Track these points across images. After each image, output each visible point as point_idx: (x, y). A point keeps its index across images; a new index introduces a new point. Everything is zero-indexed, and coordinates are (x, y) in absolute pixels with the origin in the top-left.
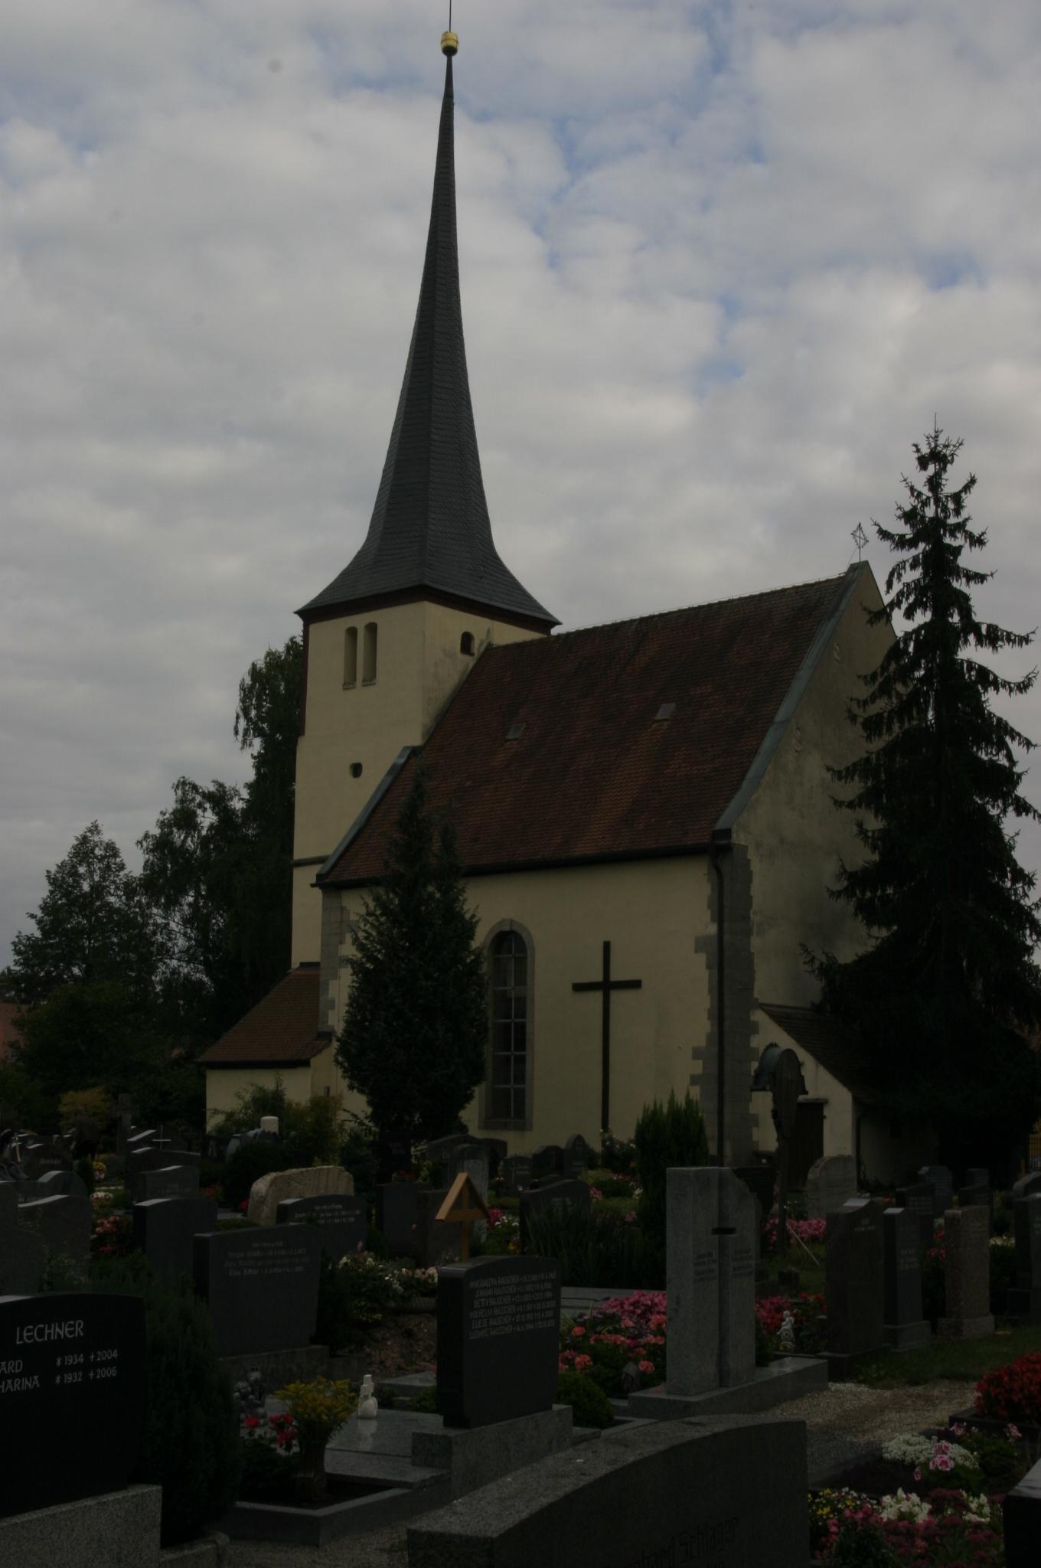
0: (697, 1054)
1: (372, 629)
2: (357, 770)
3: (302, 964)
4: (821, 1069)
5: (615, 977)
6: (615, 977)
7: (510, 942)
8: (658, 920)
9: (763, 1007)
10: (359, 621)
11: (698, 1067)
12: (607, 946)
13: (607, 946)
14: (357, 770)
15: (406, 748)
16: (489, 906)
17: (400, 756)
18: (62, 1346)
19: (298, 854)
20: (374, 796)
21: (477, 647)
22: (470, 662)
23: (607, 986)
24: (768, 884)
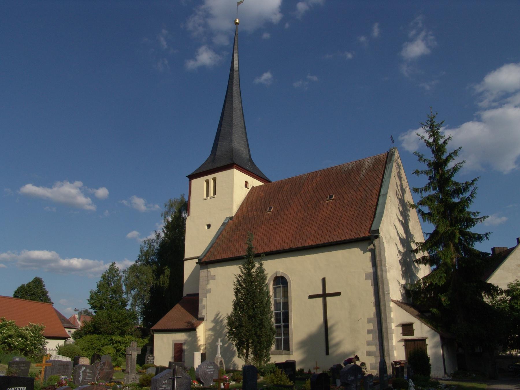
0: (370, 321)
1: (215, 180)
2: (209, 226)
3: (187, 295)
4: (423, 324)
5: (328, 291)
6: (328, 291)
7: (281, 281)
8: (346, 266)
9: (393, 301)
10: (210, 177)
11: (371, 326)
12: (324, 280)
13: (324, 280)
14: (209, 226)
15: (227, 218)
16: (272, 267)
17: (225, 220)
18: (46, 359)
19: (186, 256)
20: (216, 234)
21: (250, 186)
22: (248, 190)
23: (324, 295)
24: (391, 252)
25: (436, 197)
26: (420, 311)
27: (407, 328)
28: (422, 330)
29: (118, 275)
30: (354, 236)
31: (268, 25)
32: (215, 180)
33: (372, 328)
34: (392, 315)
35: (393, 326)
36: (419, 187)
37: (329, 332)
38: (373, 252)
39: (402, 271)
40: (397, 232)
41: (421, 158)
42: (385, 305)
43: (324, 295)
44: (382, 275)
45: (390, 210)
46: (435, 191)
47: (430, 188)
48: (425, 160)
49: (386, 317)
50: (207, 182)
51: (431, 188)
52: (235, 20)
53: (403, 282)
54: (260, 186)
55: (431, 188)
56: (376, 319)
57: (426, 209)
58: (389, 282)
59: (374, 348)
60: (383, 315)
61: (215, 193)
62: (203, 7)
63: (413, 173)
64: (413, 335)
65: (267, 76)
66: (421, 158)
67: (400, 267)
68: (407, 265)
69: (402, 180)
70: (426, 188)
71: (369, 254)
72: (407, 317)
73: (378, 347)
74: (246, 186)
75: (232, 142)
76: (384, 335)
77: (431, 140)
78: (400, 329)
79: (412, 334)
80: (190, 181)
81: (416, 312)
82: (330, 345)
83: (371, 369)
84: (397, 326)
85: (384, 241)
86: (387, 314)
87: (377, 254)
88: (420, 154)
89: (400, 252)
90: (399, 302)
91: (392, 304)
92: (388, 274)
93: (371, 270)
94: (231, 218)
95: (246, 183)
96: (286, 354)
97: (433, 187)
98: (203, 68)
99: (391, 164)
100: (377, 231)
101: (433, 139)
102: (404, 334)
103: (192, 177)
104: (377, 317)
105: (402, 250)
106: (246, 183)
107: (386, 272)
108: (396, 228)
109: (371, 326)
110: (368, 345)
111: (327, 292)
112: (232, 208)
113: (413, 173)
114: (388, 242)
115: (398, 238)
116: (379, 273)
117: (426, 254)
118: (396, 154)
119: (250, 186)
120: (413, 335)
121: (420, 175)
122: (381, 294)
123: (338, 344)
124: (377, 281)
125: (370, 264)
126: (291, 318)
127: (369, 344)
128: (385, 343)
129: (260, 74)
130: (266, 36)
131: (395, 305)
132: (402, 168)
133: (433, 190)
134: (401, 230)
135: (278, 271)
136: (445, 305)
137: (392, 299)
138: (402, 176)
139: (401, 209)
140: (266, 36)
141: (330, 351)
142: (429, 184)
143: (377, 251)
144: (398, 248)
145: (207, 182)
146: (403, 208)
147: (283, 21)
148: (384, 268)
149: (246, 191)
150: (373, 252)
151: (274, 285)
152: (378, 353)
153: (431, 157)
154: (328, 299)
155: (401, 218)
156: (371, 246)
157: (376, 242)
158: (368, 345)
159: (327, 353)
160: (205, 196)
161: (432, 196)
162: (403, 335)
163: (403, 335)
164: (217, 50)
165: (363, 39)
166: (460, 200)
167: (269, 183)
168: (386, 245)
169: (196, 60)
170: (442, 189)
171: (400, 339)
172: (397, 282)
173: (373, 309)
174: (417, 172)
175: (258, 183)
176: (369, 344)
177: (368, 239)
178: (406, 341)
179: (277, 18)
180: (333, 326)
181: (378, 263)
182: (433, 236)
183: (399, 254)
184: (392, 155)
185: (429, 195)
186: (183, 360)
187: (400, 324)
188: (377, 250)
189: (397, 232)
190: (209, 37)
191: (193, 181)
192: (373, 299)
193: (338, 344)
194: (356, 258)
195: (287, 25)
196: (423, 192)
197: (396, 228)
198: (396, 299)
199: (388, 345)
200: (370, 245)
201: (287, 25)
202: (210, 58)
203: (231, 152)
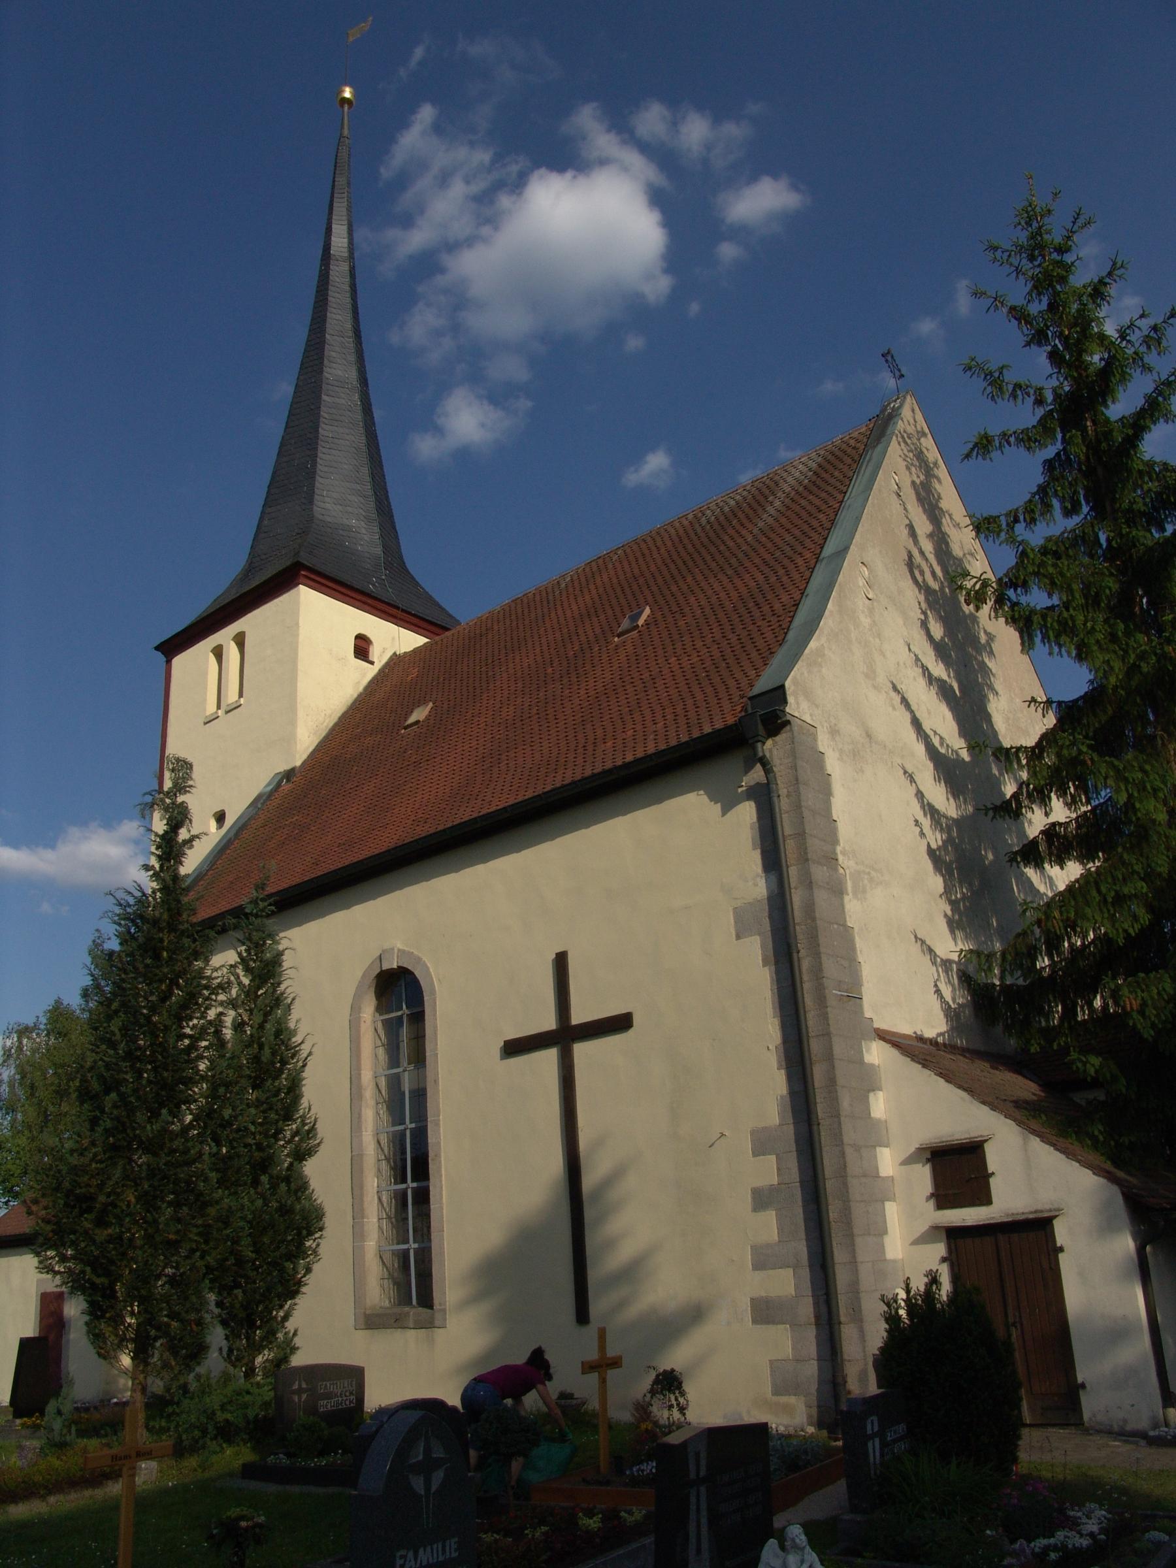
1: (240, 640)
4: (1035, 1143)
8: (652, 883)
9: (883, 1036)
10: (224, 636)
12: (561, 962)
13: (561, 962)
22: (370, 671)
23: (565, 1036)
25: (1081, 540)
26: (1046, 1085)
27: (957, 1169)
28: (1031, 1174)
31: (635, 312)
32: (240, 640)
33: (775, 1181)
34: (879, 1106)
35: (887, 1162)
36: (999, 507)
37: (589, 1214)
38: (764, 797)
39: (953, 903)
40: (916, 723)
41: (995, 382)
42: (829, 1057)
43: (565, 1036)
44: (810, 908)
45: (865, 621)
46: (1076, 520)
47: (1048, 507)
48: (1018, 386)
49: (836, 1115)
50: (218, 652)
51: (1056, 503)
53: (950, 947)
54: (416, 651)
55: (1056, 503)
56: (790, 1129)
57: (1037, 598)
58: (859, 943)
59: (786, 1283)
60: (821, 1109)
62: (440, 280)
63: (968, 456)
64: (988, 1201)
65: (657, 461)
66: (995, 382)
67: (937, 883)
68: (973, 863)
69: (946, 521)
70: (1031, 513)
71: (747, 812)
72: (955, 1114)
73: (806, 1273)
75: (311, 502)
76: (833, 1212)
77: (1037, 307)
78: (923, 1177)
79: (983, 1197)
80: (169, 662)
81: (1026, 1088)
82: (594, 1275)
83: (777, 1392)
84: (908, 1161)
85: (824, 743)
86: (845, 1103)
87: (783, 804)
88: (993, 366)
89: (931, 811)
90: (933, 1042)
91: (876, 1054)
92: (853, 907)
93: (758, 888)
95: (362, 647)
96: (419, 1326)
97: (1062, 500)
98: (464, 455)
99: (879, 448)
101: (1045, 300)
102: (944, 1197)
103: (173, 646)
104: (796, 1124)
105: (949, 807)
106: (362, 647)
107: (838, 891)
108: (905, 702)
109: (766, 1171)
110: (759, 1266)
111: (577, 1019)
113: (968, 456)
114: (855, 755)
115: (920, 749)
116: (797, 899)
117: (1060, 812)
118: (906, 412)
119: (380, 655)
120: (988, 1201)
121: (995, 454)
122: (809, 1000)
123: (631, 1273)
124: (794, 943)
125: (755, 861)
126: (438, 1155)
127: (763, 1260)
128: (839, 1256)
129: (637, 458)
130: (634, 343)
131: (894, 1053)
132: (942, 472)
133: (1068, 513)
134: (942, 723)
135: (387, 946)
136: (1148, 1034)
137: (880, 1024)
138: (944, 504)
139: (937, 631)
140: (634, 343)
141: (597, 1307)
142: (1042, 490)
143: (783, 792)
144: (920, 795)
145: (218, 652)
146: (945, 621)
147: (677, 297)
148: (819, 873)
149: (360, 675)
150: (764, 797)
151: (380, 1009)
152: (806, 1309)
153: (1037, 368)
154: (582, 1051)
155: (939, 670)
156: (757, 775)
158: (759, 1266)
159: (582, 1316)
160: (211, 708)
161: (1059, 540)
162: (940, 1206)
163: (940, 1206)
164: (498, 396)
165: (926, 327)
167: (448, 634)
168: (833, 765)
169: (439, 431)
170: (1103, 501)
171: (923, 1227)
172: (916, 948)
173: (777, 1083)
174: (984, 445)
175: (410, 641)
176: (763, 1260)
177: (735, 740)
178: (954, 1234)
179: (659, 287)
180: (609, 1182)
181: (789, 848)
182: (1070, 715)
183: (926, 823)
184: (893, 415)
185: (1048, 539)
186: (436, 1301)
187: (921, 1150)
188: (782, 787)
189: (916, 723)
190: (471, 364)
191: (178, 661)
192: (771, 1031)
193: (631, 1273)
194: (692, 841)
195: (694, 308)
196: (1020, 528)
197: (905, 702)
198: (905, 1028)
199: (853, 1263)
200: (748, 768)
201: (694, 308)
202: (483, 425)
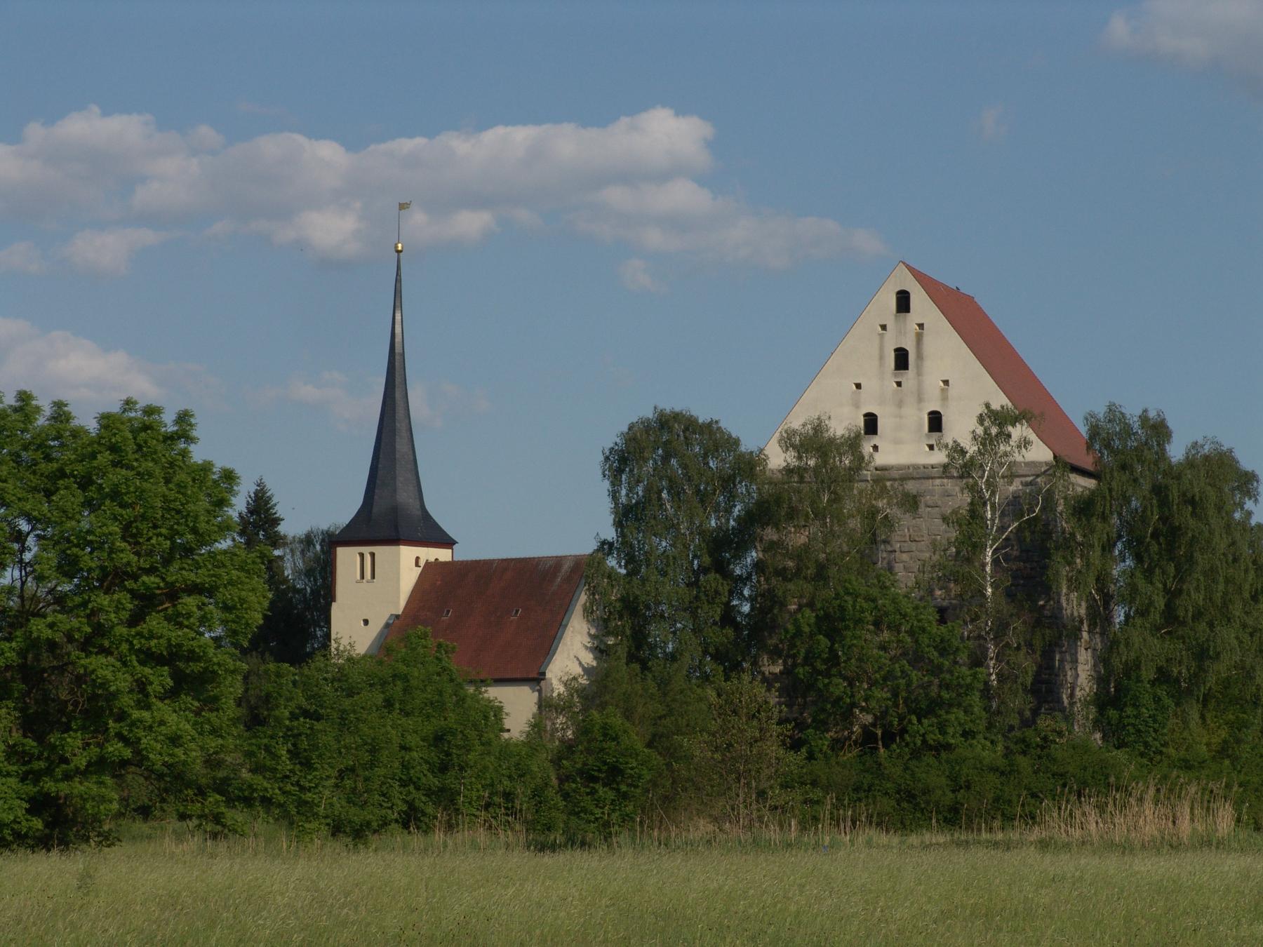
1: (373, 555)
2: (366, 622)
10: (366, 550)
22: (420, 570)
29: (878, 824)
30: (525, 676)
32: (373, 555)
50: (362, 555)
52: (396, 247)
61: (373, 577)
71: (536, 694)
74: (417, 565)
94: (397, 617)
100: (544, 674)
112: (398, 602)
119: (422, 563)
145: (362, 555)
157: (543, 683)
160: (358, 577)
166: (940, 457)
203: (395, 511)
